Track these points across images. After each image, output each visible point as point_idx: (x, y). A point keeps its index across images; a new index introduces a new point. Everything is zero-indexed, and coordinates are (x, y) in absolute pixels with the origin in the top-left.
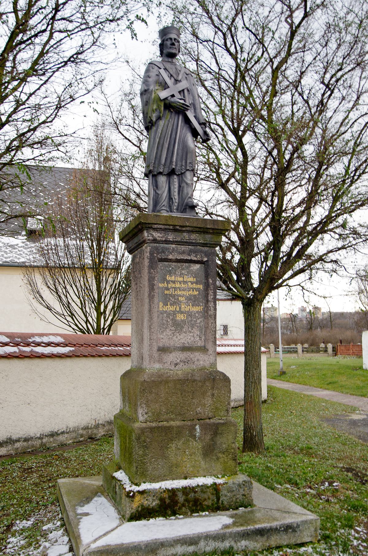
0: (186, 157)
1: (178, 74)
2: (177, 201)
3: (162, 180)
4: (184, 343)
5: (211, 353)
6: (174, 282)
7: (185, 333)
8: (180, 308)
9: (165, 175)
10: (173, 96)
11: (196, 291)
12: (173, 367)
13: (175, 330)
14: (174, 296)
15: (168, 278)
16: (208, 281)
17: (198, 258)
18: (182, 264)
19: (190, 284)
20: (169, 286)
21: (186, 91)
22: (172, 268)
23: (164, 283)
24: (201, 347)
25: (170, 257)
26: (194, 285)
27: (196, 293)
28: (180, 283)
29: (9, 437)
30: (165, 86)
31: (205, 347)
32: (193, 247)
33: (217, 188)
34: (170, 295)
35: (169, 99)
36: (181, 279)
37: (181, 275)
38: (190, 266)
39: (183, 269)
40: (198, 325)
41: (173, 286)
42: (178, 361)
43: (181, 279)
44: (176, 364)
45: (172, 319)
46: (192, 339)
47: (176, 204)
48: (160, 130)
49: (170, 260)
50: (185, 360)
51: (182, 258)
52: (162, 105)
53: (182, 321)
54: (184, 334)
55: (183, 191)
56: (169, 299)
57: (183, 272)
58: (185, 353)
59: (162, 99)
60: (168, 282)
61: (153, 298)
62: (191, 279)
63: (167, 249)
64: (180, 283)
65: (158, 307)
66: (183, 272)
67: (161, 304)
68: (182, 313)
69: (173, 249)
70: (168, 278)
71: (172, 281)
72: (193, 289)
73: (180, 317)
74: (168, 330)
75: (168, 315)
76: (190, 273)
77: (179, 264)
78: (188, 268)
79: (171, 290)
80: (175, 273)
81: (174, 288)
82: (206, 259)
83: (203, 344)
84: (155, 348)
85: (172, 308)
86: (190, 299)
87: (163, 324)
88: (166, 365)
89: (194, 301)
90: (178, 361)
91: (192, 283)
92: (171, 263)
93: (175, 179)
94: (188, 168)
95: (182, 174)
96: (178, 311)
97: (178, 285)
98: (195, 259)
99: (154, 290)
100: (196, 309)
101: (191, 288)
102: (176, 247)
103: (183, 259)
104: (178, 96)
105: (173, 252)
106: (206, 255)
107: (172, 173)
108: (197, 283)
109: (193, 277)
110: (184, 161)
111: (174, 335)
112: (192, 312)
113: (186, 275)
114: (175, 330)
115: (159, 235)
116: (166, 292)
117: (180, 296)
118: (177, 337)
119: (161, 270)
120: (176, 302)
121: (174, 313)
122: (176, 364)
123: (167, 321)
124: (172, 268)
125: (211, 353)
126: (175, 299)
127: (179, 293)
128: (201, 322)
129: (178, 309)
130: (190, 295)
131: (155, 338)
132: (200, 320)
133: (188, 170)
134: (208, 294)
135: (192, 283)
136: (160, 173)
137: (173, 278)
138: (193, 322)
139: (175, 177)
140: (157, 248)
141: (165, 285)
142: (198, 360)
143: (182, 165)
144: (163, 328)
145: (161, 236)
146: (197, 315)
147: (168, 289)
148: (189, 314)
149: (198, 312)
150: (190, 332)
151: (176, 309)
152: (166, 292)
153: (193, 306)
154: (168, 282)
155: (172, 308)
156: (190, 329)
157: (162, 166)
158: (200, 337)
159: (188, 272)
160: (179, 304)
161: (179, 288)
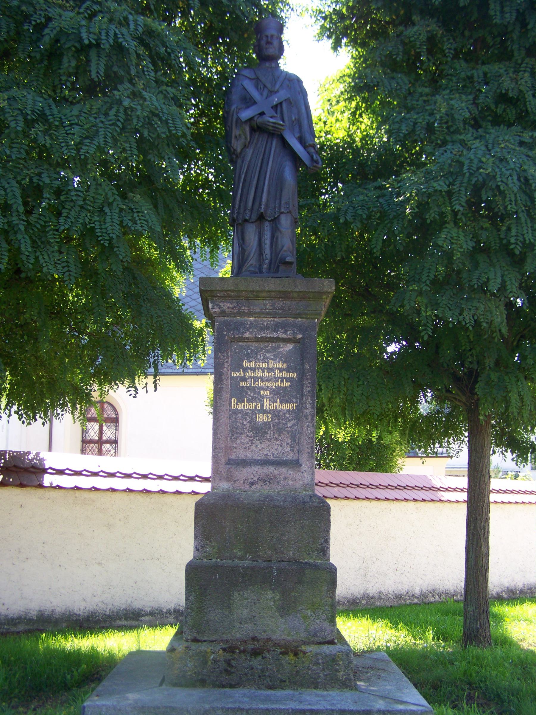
0: (281, 195)
1: (276, 82)
2: (268, 256)
3: (251, 231)
4: (267, 455)
5: (306, 468)
6: (253, 370)
7: (270, 440)
8: (262, 406)
9: (252, 222)
10: (262, 114)
11: (287, 382)
12: (248, 487)
13: (254, 437)
14: (253, 389)
15: (245, 364)
16: (303, 366)
17: (289, 334)
18: (266, 344)
19: (277, 372)
20: (247, 375)
21: (284, 105)
22: (252, 350)
23: (239, 371)
24: (292, 461)
25: (247, 335)
26: (284, 372)
27: (286, 384)
28: (263, 370)
29: (129, 602)
30: (248, 101)
31: (298, 460)
32: (281, 320)
33: (281, 232)
34: (249, 388)
35: (255, 119)
36: (265, 365)
37: (265, 360)
38: (279, 347)
39: (268, 351)
40: (289, 429)
41: (253, 375)
42: (255, 479)
43: (265, 365)
44: (252, 484)
45: (250, 422)
46: (280, 449)
47: (267, 261)
48: (246, 164)
49: (248, 338)
50: (266, 478)
51: (264, 335)
52: (247, 129)
53: (264, 423)
54: (267, 442)
55: (277, 242)
56: (247, 394)
57: (268, 355)
58: (265, 468)
59: (243, 120)
60: (245, 370)
61: (220, 392)
62: (280, 365)
63: (243, 324)
64: (263, 370)
65: (230, 405)
66: (268, 355)
67: (234, 401)
68: (264, 412)
69: (251, 323)
70: (245, 364)
71: (251, 369)
72: (282, 379)
73: (261, 418)
74: (243, 437)
75: (245, 414)
76: (278, 357)
77: (262, 345)
78: (274, 349)
79: (249, 380)
80: (256, 358)
81: (254, 377)
82: (300, 336)
83: (295, 458)
84: (223, 460)
85: (252, 406)
86: (278, 393)
87: (237, 428)
88: (237, 484)
89: (284, 396)
90: (255, 479)
91: (281, 370)
92: (248, 344)
93: (267, 227)
94: (283, 210)
95: (275, 218)
96: (259, 410)
97: (260, 374)
98: (284, 336)
99: (222, 380)
100: (286, 407)
101: (279, 378)
102: (255, 321)
103: (267, 338)
104: (269, 112)
105: (250, 327)
106: (301, 331)
107: (261, 218)
108: (288, 370)
109: (283, 363)
110: (278, 201)
111: (252, 443)
112: (280, 411)
113: (272, 359)
114: (254, 437)
115: (228, 305)
116: (242, 384)
117: (262, 389)
118: (256, 447)
119: (236, 353)
120: (257, 398)
121: (254, 412)
122: (252, 484)
123: (243, 424)
124: (252, 350)
125: (306, 468)
126: (255, 393)
127: (260, 384)
128: (293, 425)
129: (259, 407)
130: (279, 388)
131: (223, 446)
132: (292, 422)
133: (282, 213)
134: (303, 385)
135: (281, 370)
136: (246, 221)
137: (253, 365)
138: (281, 426)
139: (267, 223)
140: (227, 324)
141: (241, 374)
142: (285, 479)
143: (275, 208)
144: (237, 433)
145: (231, 306)
146: (287, 415)
147: (244, 379)
148: (275, 414)
149: (289, 411)
150: (277, 440)
151: (256, 406)
152: (242, 384)
153: (281, 402)
154: (245, 370)
155: (252, 406)
156: (276, 436)
157: (248, 212)
158: (291, 447)
159: (274, 355)
160: (260, 401)
161: (262, 378)
